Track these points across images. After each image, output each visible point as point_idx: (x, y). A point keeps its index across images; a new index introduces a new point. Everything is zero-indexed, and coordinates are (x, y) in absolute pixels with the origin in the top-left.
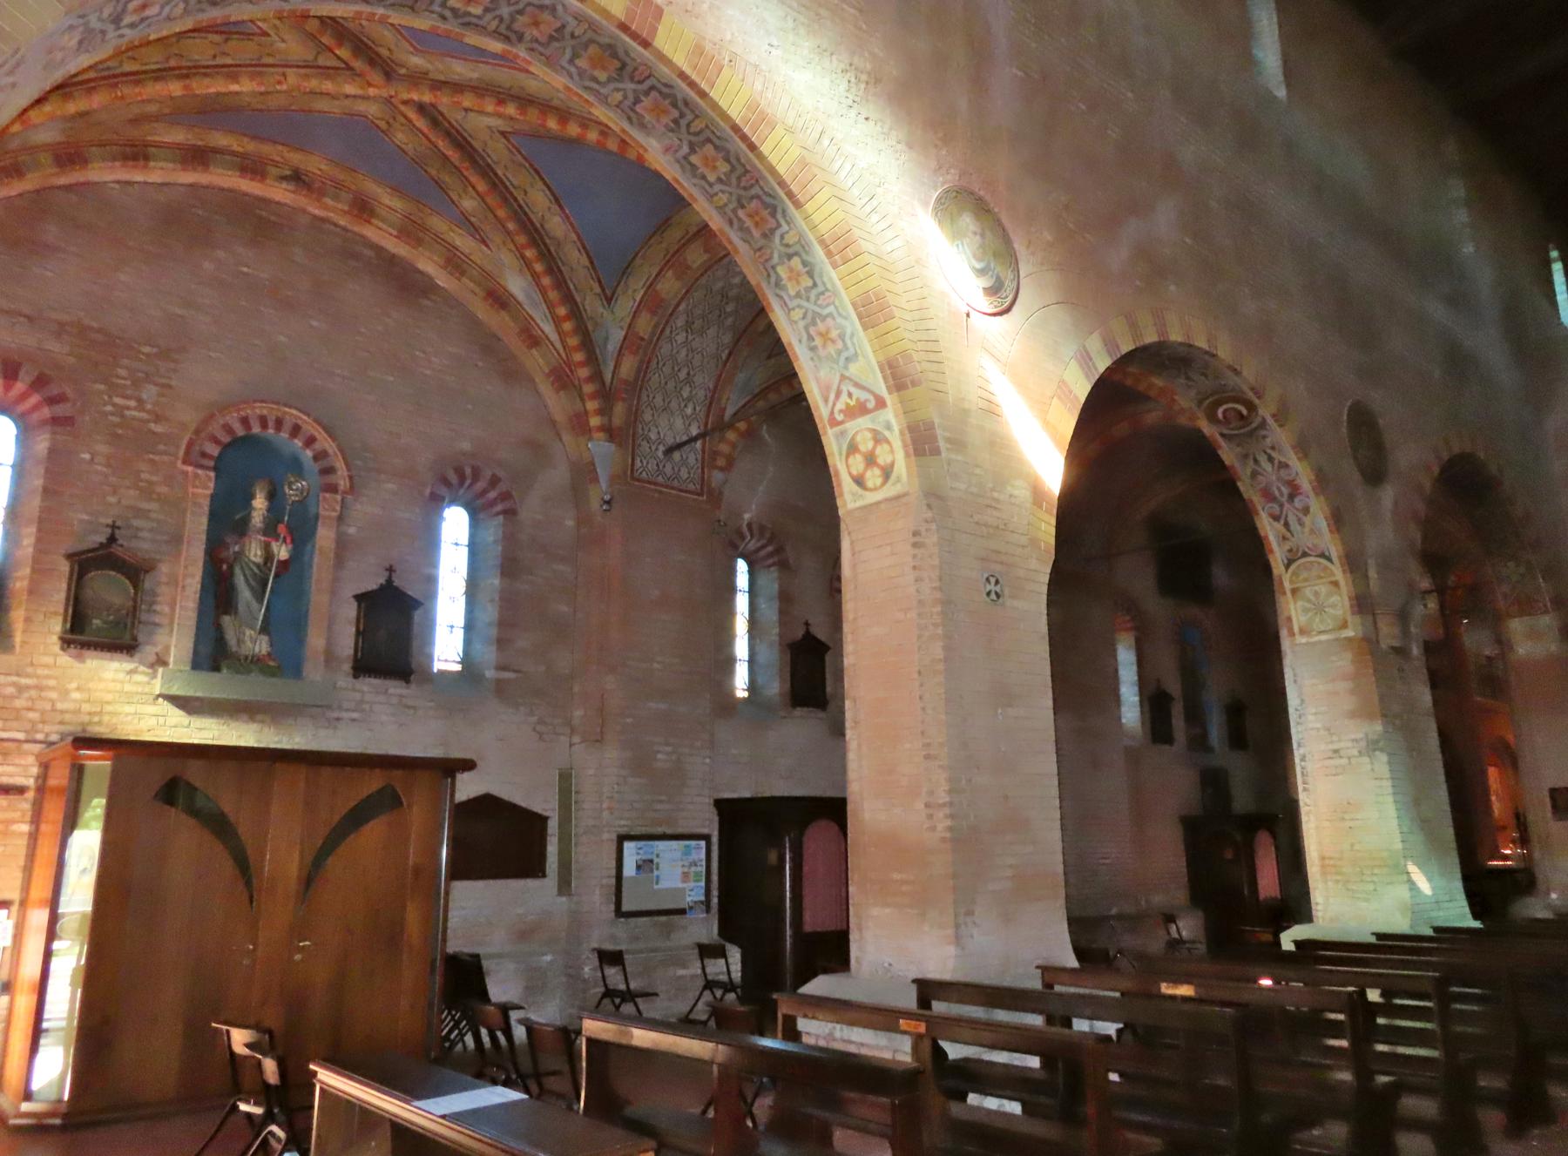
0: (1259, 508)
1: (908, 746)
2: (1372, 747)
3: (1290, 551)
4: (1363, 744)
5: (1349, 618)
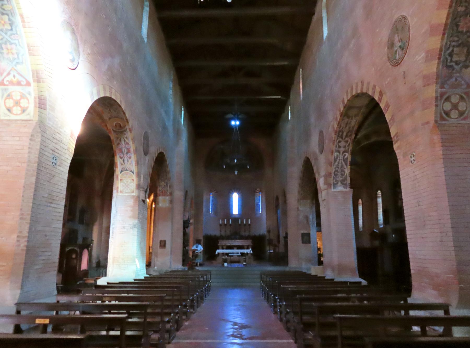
1: (13, 213)
2: (134, 226)
3: (123, 168)
4: (132, 226)
5: (135, 190)
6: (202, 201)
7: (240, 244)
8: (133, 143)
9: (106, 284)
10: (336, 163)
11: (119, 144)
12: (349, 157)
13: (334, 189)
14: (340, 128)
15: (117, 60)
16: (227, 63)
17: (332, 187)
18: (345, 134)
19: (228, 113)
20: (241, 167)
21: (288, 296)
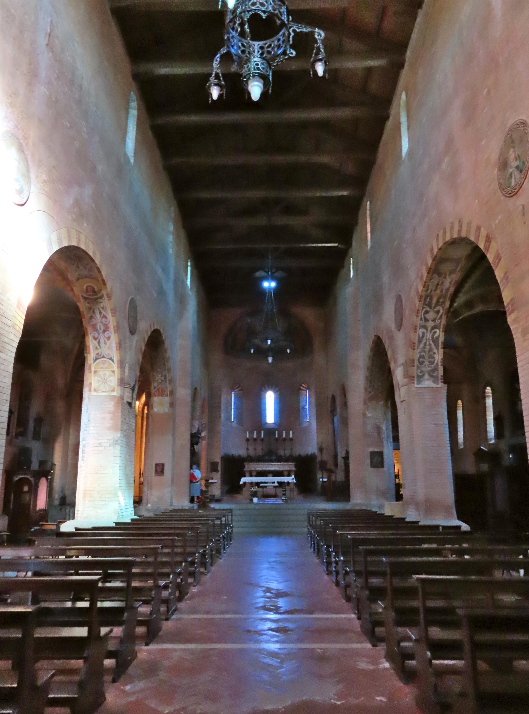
0: (89, 333)
2: (116, 442)
3: (98, 354)
4: (112, 441)
5: (116, 387)
6: (220, 403)
7: (278, 469)
8: (112, 316)
9: (74, 530)
10: (422, 345)
11: (91, 317)
12: (441, 336)
13: (418, 384)
14: (427, 290)
15: (88, 191)
16: (256, 194)
17: (416, 382)
18: (434, 301)
19: (258, 270)
20: (278, 352)
21: (348, 548)
